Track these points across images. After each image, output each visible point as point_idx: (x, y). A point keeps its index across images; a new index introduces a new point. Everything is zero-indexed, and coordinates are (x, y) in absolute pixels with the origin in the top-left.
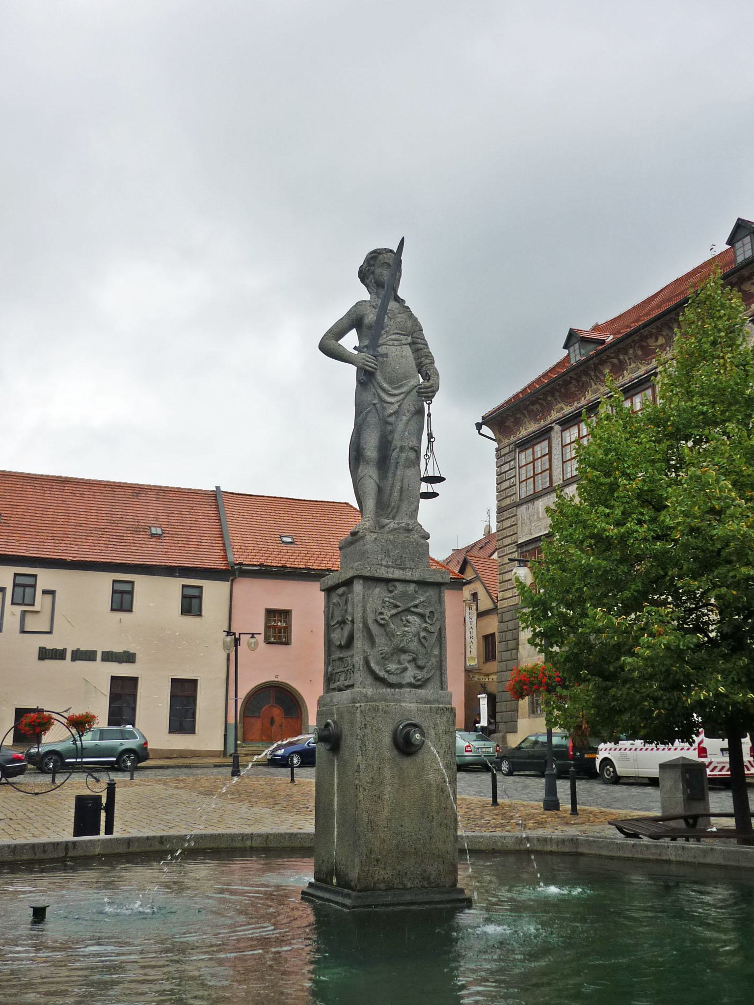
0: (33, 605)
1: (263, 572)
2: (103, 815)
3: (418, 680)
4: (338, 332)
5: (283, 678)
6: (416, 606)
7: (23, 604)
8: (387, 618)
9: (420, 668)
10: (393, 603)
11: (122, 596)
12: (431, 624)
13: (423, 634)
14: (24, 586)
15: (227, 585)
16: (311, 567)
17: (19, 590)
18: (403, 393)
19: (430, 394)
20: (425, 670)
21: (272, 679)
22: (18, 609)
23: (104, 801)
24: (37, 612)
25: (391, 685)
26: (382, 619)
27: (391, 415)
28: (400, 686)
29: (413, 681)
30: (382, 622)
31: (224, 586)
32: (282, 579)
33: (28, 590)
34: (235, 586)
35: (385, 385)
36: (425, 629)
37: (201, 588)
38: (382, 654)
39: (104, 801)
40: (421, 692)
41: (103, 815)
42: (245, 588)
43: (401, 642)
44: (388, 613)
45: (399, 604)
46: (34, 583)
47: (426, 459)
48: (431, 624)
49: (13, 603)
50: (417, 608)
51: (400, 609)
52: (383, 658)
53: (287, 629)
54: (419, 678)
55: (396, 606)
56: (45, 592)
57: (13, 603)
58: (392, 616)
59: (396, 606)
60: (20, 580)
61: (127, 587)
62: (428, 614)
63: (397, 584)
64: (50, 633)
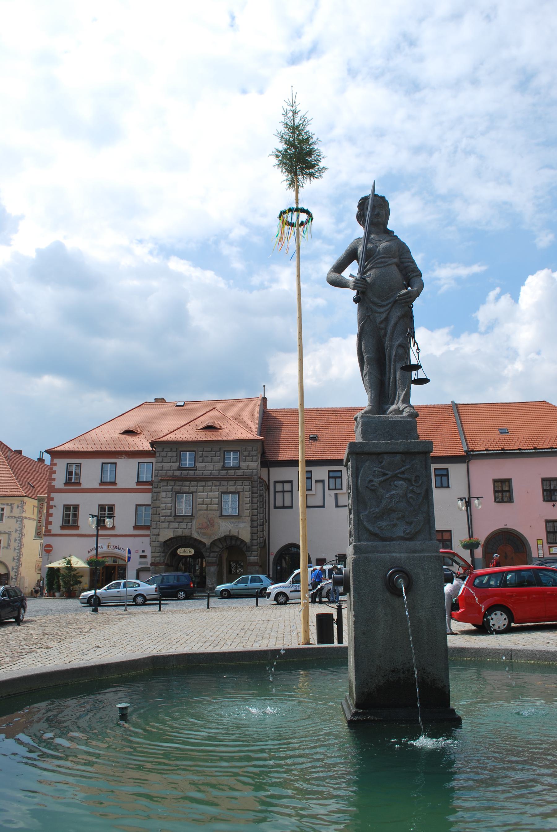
0: (342, 489)
1: (488, 455)
2: (335, 626)
3: (408, 534)
4: (340, 267)
5: (511, 525)
6: (403, 473)
7: (335, 489)
8: (377, 485)
9: (410, 523)
10: (381, 472)
11: (335, 481)
12: (417, 487)
13: (410, 495)
14: (335, 478)
15: (464, 466)
16: (522, 448)
17: (332, 481)
18: (390, 303)
19: (408, 300)
20: (413, 525)
21: (502, 526)
22: (333, 493)
23: (335, 617)
24: (314, 494)
25: (383, 539)
26: (373, 485)
27: (381, 322)
28: (391, 539)
29: (402, 535)
30: (373, 488)
31: (462, 467)
32: (489, 459)
33: (337, 480)
34: (470, 465)
35: (375, 299)
36: (412, 491)
37: (447, 469)
38: (374, 513)
39: (335, 617)
40: (411, 544)
41: (335, 626)
42: (476, 466)
43: (389, 503)
44: (377, 480)
45: (387, 472)
46: (310, 476)
47: (418, 353)
48: (417, 487)
49: (329, 489)
50: (404, 474)
51: (387, 477)
52: (375, 517)
53: (510, 491)
54: (407, 531)
55: (385, 474)
56: (317, 481)
57: (329, 489)
58: (381, 482)
59: (385, 474)
60: (438, 472)
61: (444, 472)
62: (414, 479)
63: (385, 456)
64: (323, 506)
